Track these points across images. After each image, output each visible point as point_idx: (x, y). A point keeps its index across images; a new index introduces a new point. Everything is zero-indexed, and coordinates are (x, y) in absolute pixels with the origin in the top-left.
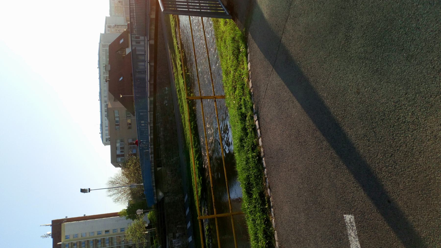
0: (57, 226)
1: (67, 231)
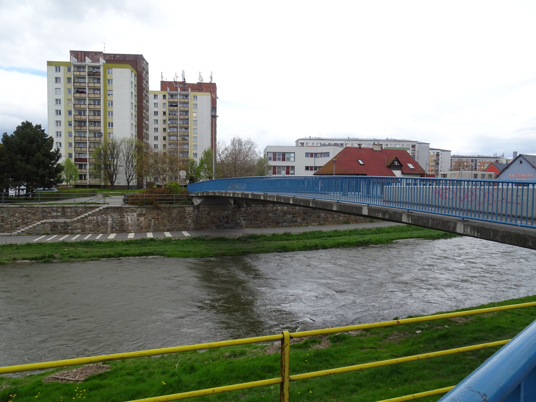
0: (210, 88)
1: (204, 98)
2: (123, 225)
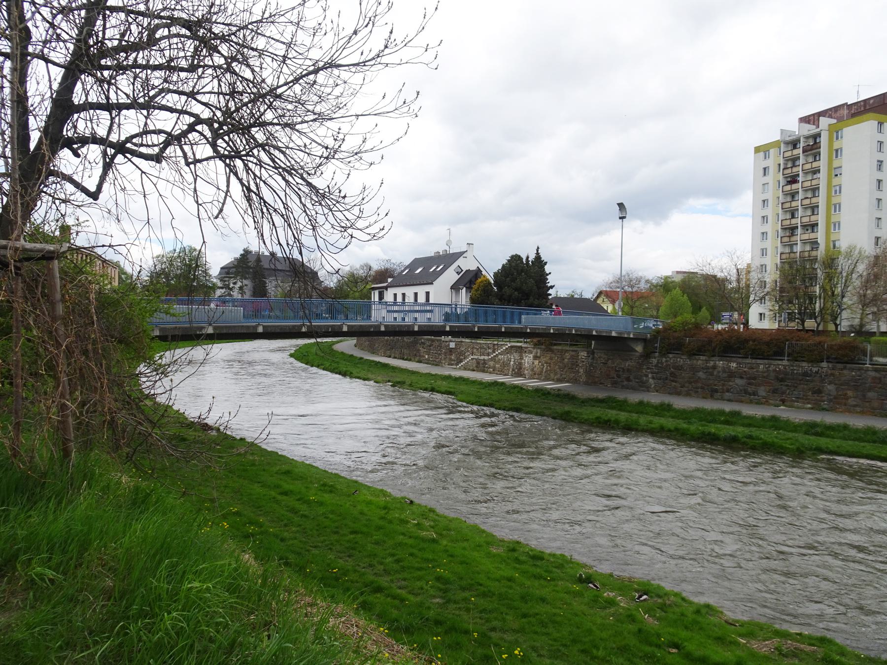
2: (521, 368)
